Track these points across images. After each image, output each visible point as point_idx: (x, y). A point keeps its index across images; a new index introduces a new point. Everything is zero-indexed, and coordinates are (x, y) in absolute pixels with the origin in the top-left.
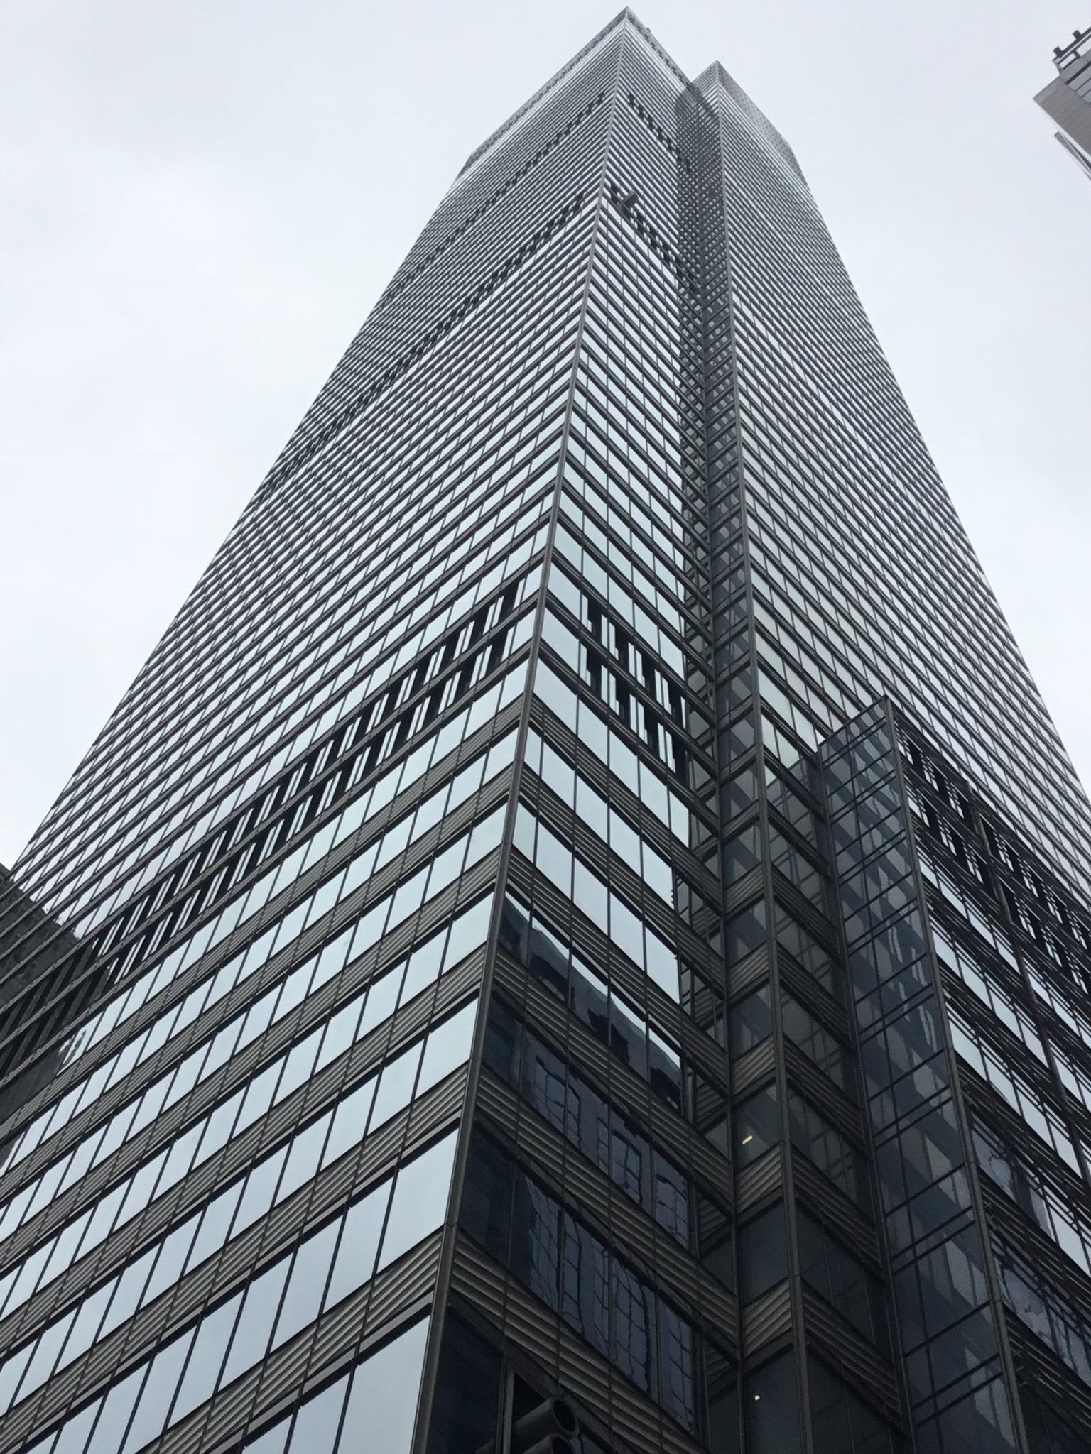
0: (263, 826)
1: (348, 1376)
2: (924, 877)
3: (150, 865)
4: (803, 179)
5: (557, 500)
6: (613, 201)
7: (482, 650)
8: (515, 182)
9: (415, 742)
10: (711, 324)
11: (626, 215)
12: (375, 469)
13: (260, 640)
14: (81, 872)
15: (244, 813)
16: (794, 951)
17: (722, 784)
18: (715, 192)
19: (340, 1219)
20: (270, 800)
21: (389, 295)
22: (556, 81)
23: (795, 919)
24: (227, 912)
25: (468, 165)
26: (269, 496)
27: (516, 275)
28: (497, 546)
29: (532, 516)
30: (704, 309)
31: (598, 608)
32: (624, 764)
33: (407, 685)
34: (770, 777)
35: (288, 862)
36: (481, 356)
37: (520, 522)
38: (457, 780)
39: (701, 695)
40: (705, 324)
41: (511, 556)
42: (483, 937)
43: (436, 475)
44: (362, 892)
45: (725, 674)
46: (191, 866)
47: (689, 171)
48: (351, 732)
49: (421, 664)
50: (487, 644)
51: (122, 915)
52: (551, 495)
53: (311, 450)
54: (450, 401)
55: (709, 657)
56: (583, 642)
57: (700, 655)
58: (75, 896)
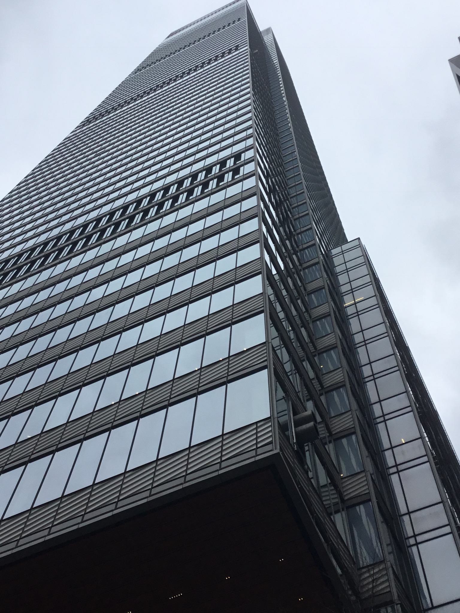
1: (52, 455)
7: (110, 226)
8: (150, 65)
9: (106, 240)
12: (74, 154)
15: (27, 252)
19: (7, 420)
27: (146, 98)
28: (100, 202)
37: (111, 195)
38: (74, 278)
41: (91, 213)
44: (60, 296)
50: (84, 238)
54: (101, 141)
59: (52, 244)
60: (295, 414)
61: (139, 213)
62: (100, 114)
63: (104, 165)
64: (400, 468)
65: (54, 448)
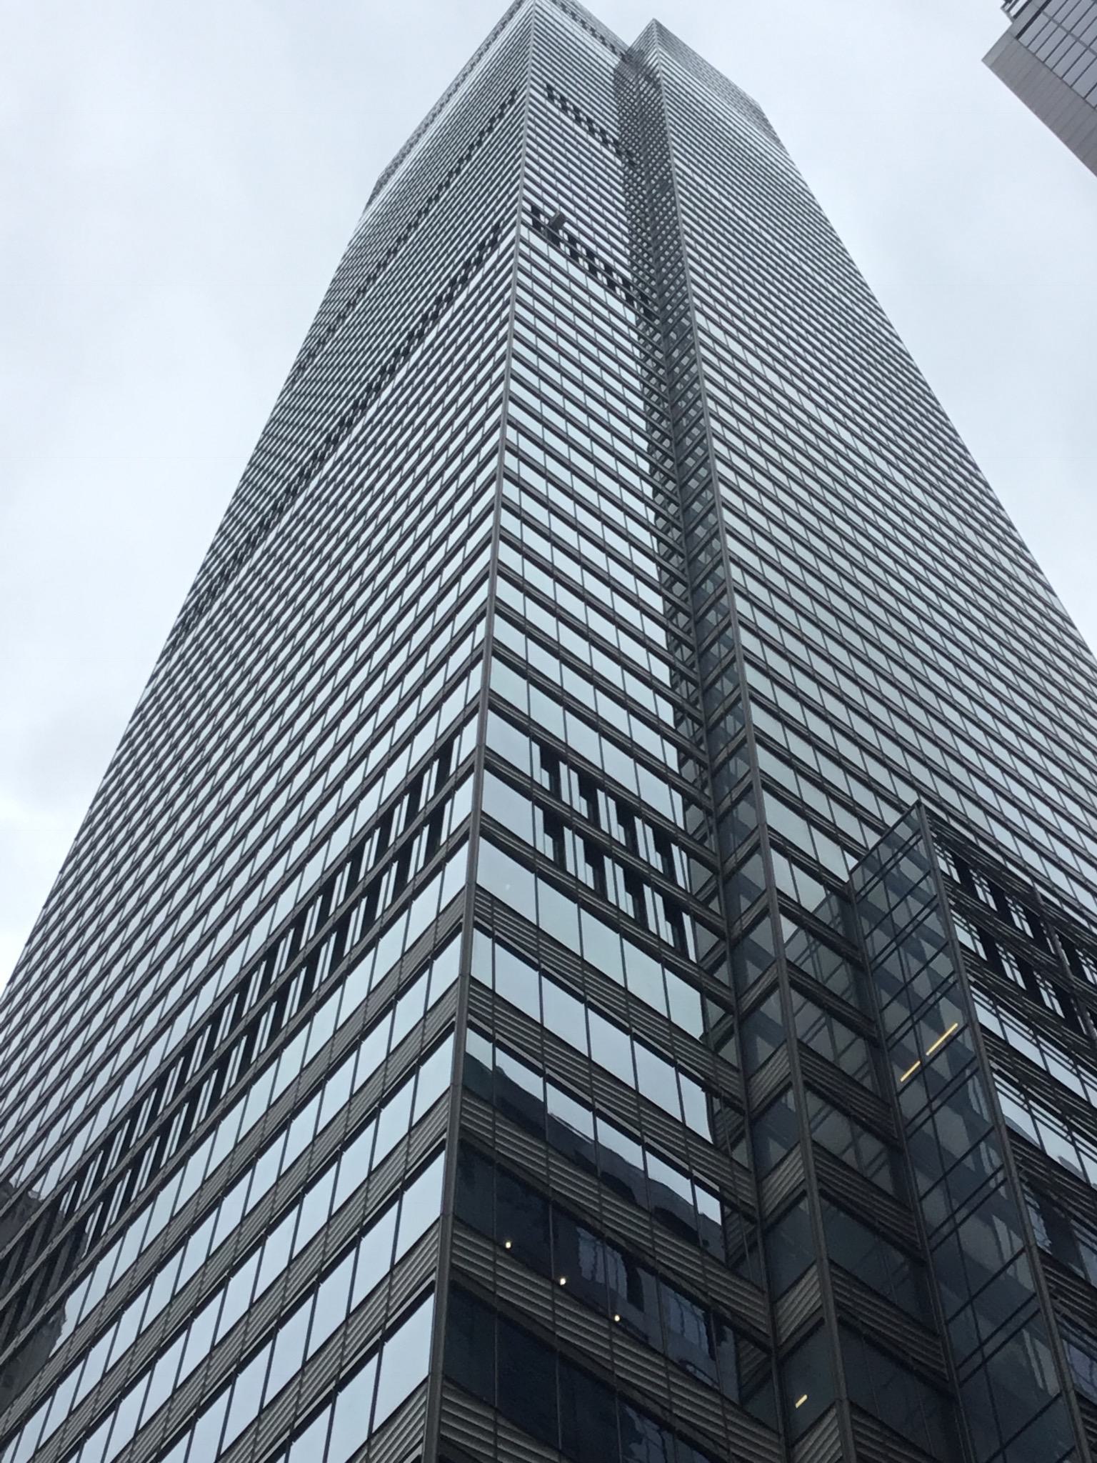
0: (224, 1047)
2: (983, 1028)
3: (126, 1081)
4: (778, 141)
5: (490, 627)
6: (536, 227)
9: (418, 883)
10: (676, 354)
11: (554, 241)
13: (227, 736)
14: (68, 1076)
15: (228, 1000)
16: (834, 1146)
17: (733, 943)
18: (666, 186)
20: (284, 948)
21: (300, 367)
22: (465, 75)
23: (836, 1106)
24: (255, 1089)
25: (376, 192)
26: (183, 642)
29: (464, 651)
30: (666, 336)
31: (553, 754)
32: (602, 948)
33: (400, 814)
34: (788, 928)
36: (435, 400)
39: (698, 837)
40: (668, 356)
42: (436, 1212)
43: (422, 527)
45: (727, 802)
46: (174, 1076)
47: (631, 164)
48: (371, 848)
49: (383, 821)
51: (100, 1148)
52: (483, 623)
53: (239, 561)
55: (704, 785)
56: (537, 803)
57: (692, 784)
58: (44, 1133)
59: (400, 814)
62: (355, 406)
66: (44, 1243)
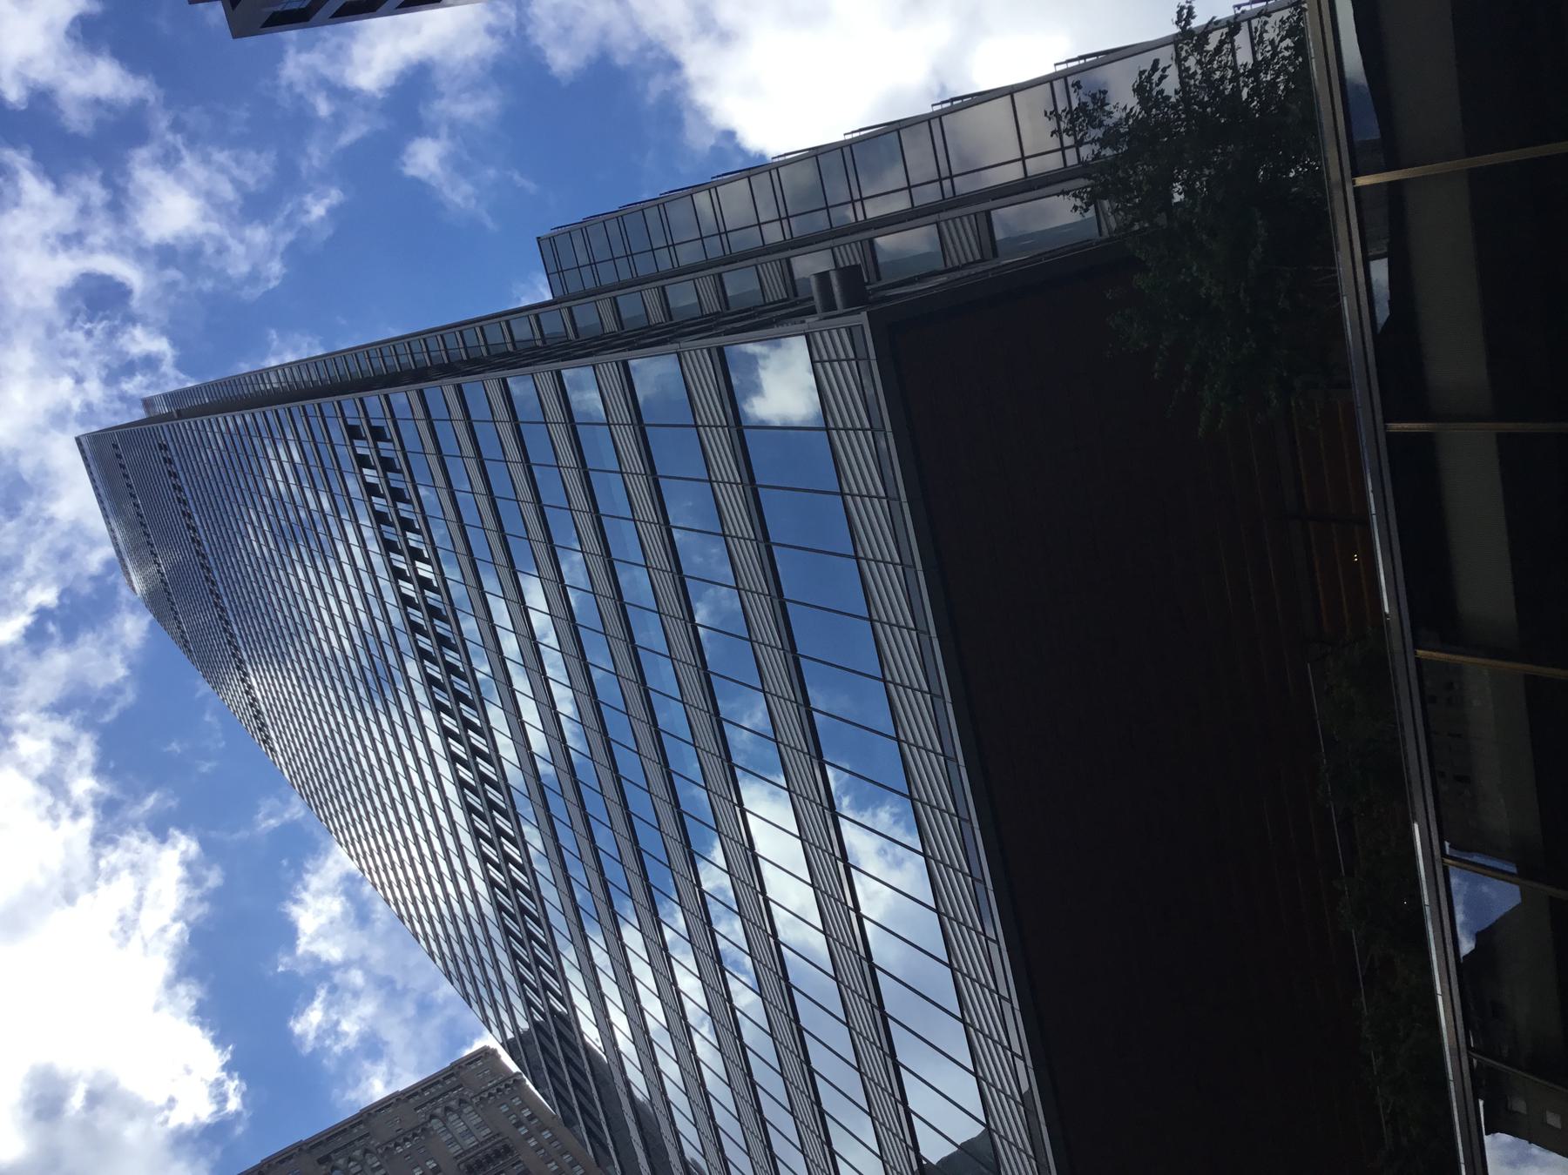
13: (420, 916)
15: (517, 967)
33: (487, 849)
35: (576, 1001)
43: (383, 755)
49: (477, 834)
59: (494, 873)
60: (812, 311)
61: (451, 683)
63: (369, 779)
64: (945, 173)
65: (865, 964)
66: (558, 1063)
